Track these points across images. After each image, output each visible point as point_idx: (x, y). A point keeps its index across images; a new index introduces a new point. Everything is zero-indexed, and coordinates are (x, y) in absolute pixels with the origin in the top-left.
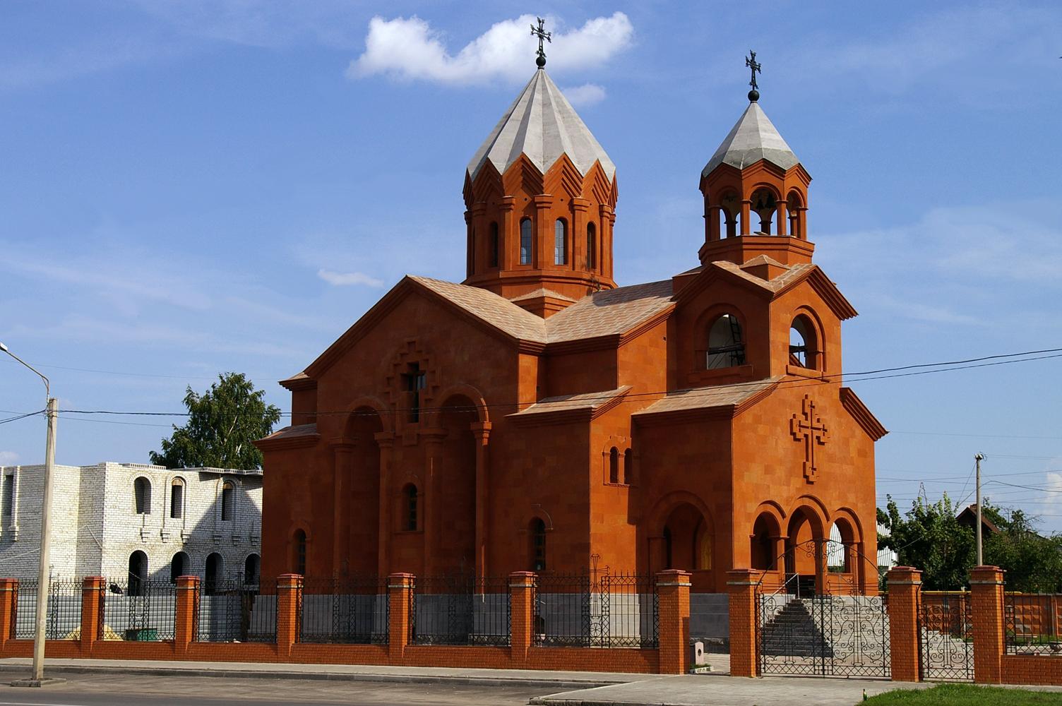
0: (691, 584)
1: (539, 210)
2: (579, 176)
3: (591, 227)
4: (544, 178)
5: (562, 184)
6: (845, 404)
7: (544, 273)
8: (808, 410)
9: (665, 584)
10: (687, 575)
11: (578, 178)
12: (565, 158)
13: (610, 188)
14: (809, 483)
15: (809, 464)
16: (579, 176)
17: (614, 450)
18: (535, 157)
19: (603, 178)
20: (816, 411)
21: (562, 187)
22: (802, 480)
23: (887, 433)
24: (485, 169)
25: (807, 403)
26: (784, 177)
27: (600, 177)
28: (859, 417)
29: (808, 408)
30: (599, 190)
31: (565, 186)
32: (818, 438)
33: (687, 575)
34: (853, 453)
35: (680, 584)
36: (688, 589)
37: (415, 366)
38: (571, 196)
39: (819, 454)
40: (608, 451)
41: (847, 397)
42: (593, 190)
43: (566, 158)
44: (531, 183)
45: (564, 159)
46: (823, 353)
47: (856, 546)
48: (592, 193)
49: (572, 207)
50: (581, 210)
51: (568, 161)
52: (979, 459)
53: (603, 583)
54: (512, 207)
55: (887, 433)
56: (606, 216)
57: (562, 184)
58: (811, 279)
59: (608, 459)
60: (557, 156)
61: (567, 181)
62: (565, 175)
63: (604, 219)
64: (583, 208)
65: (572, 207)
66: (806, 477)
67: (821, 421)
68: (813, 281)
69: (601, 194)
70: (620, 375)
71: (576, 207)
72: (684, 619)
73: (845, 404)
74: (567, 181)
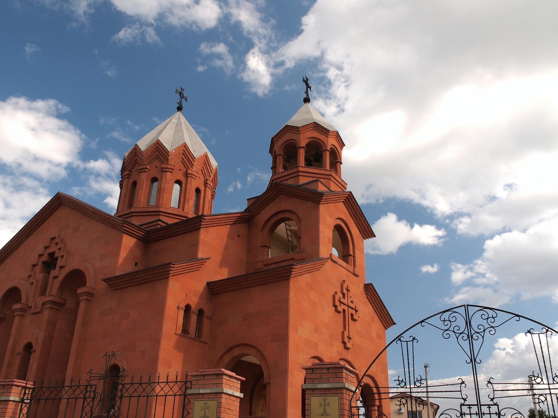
0: (242, 395)
1: (164, 173)
2: (193, 157)
3: (198, 191)
4: (170, 154)
5: (182, 161)
6: (368, 296)
7: (161, 209)
8: (345, 291)
9: (202, 391)
10: (238, 379)
11: (192, 158)
12: (185, 146)
13: (213, 173)
14: (346, 348)
15: (346, 334)
16: (193, 157)
17: (188, 308)
18: (166, 143)
19: (208, 163)
20: (350, 294)
21: (181, 163)
22: (341, 345)
23: (395, 324)
24: (134, 150)
25: (345, 286)
26: (328, 135)
27: (207, 163)
28: (376, 307)
29: (345, 291)
30: (205, 170)
31: (183, 162)
32: (352, 315)
33: (238, 379)
34: (374, 335)
35: (225, 391)
36: (237, 403)
37: (52, 255)
38: (186, 168)
39: (354, 328)
40: (183, 305)
41: (369, 289)
42: (201, 170)
43: (186, 146)
44: (162, 158)
45: (184, 146)
46: (354, 256)
47: (376, 408)
48: (201, 172)
49: (187, 175)
50: (192, 177)
51: (187, 147)
52: (426, 367)
53: (88, 394)
54: (147, 170)
55: (395, 324)
56: (208, 187)
57: (182, 161)
58: (346, 202)
59: (182, 313)
60: (181, 143)
61: (185, 160)
62: (184, 155)
63: (207, 189)
64: (193, 176)
65: (187, 175)
66: (344, 343)
67: (354, 302)
68: (347, 203)
69: (206, 174)
70: (200, 249)
71: (189, 175)
72: (22, 376)
73: (368, 296)
74: (185, 160)
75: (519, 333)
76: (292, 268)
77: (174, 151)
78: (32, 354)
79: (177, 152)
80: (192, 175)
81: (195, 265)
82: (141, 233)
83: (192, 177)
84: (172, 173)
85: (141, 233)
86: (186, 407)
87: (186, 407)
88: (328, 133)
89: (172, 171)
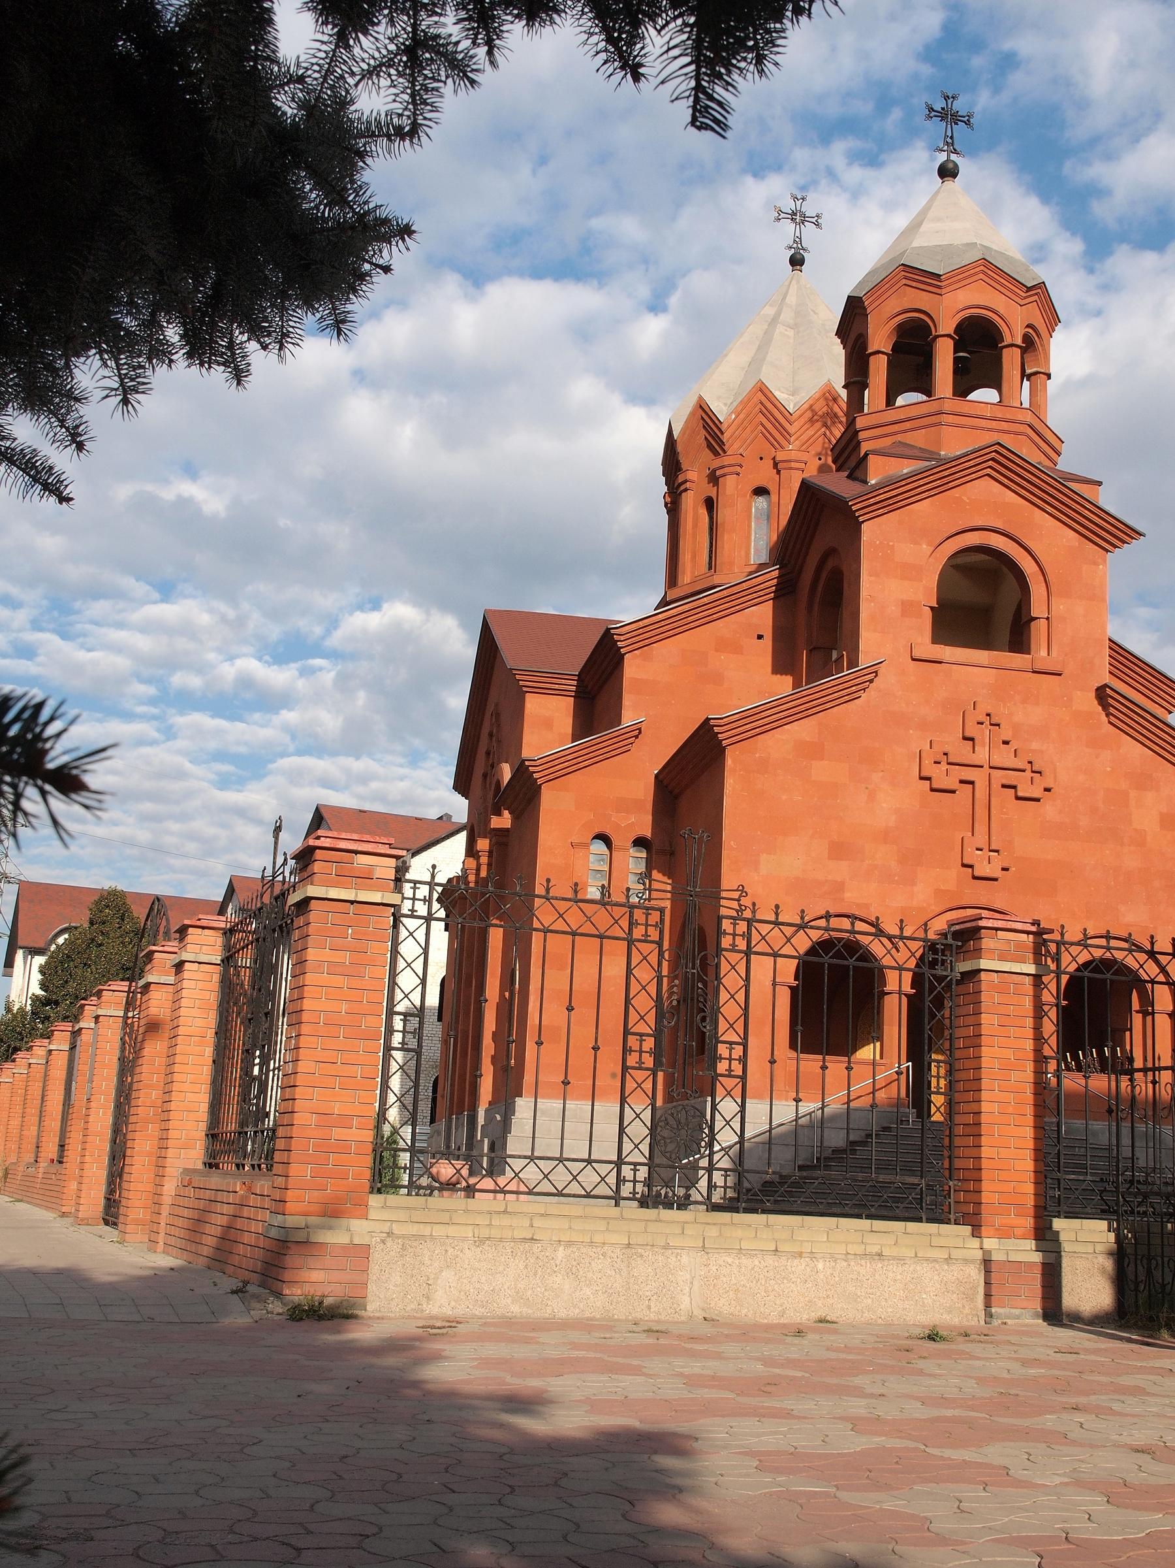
43: (764, 387)
45: (761, 390)
50: (791, 468)
61: (769, 426)
74: (769, 426)
75: (786, 675)
76: (857, 432)
77: (733, 416)
78: (868, 531)
79: (742, 416)
80: (790, 461)
81: (1060, 497)
82: (768, 577)
83: (791, 468)
84: (738, 474)
85: (768, 577)
86: (420, 981)
87: (420, 981)
88: (939, 284)
89: (738, 469)
